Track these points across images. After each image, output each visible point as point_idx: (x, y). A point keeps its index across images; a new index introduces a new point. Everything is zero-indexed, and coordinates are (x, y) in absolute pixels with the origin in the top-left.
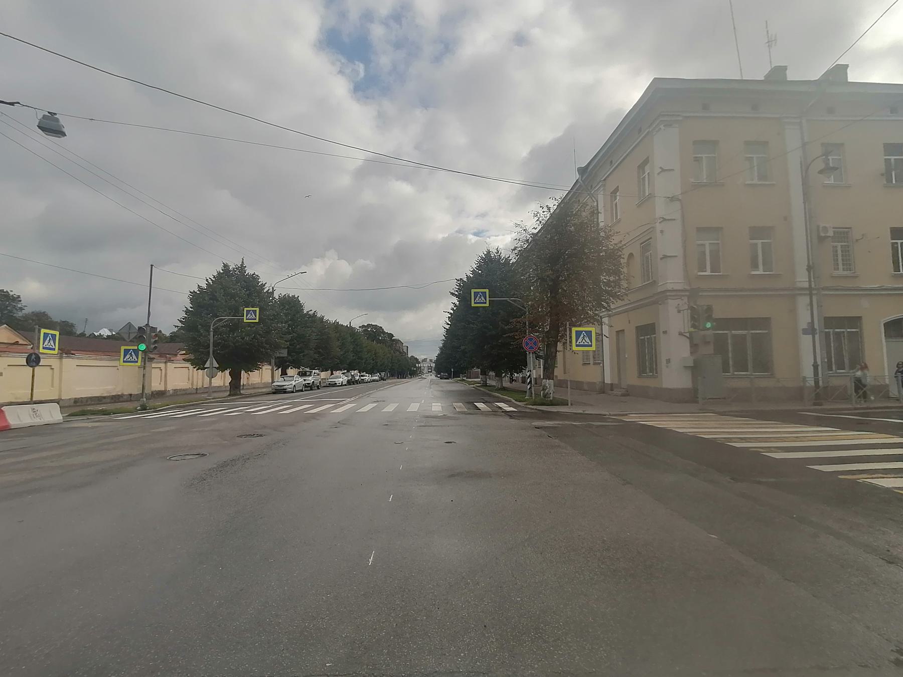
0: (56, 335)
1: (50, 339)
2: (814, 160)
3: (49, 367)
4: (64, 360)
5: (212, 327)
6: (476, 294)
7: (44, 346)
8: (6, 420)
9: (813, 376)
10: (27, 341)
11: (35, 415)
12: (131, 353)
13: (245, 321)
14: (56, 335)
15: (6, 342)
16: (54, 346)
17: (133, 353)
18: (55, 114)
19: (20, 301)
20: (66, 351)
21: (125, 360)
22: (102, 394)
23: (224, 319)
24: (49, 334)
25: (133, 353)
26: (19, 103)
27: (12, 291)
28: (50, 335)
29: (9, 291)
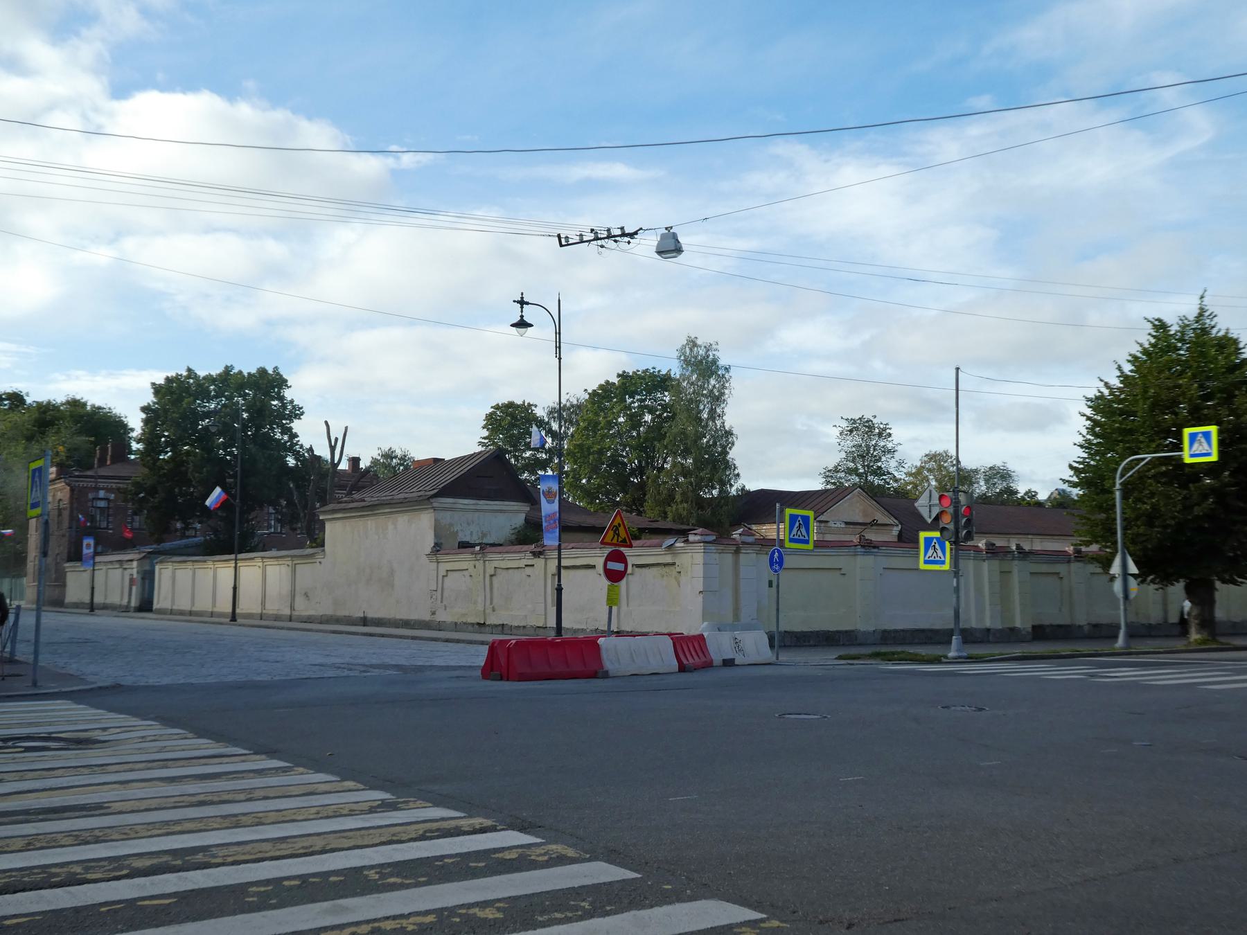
0: (809, 517)
1: (800, 524)
2: (235, 588)
3: (838, 573)
4: (170, 608)
5: (1118, 482)
6: (1193, 437)
7: (791, 536)
8: (257, 614)
9: (782, 628)
10: (892, 518)
11: (737, 648)
12: (934, 546)
13: (1188, 460)
14: (809, 517)
15: (861, 521)
16: (806, 536)
17: (937, 546)
18: (671, 228)
19: (890, 435)
20: (215, 607)
21: (927, 558)
22: (464, 615)
23: (1143, 459)
24: (798, 516)
25: (937, 546)
26: (641, 229)
27: (875, 417)
28: (799, 519)
29: (872, 419)
